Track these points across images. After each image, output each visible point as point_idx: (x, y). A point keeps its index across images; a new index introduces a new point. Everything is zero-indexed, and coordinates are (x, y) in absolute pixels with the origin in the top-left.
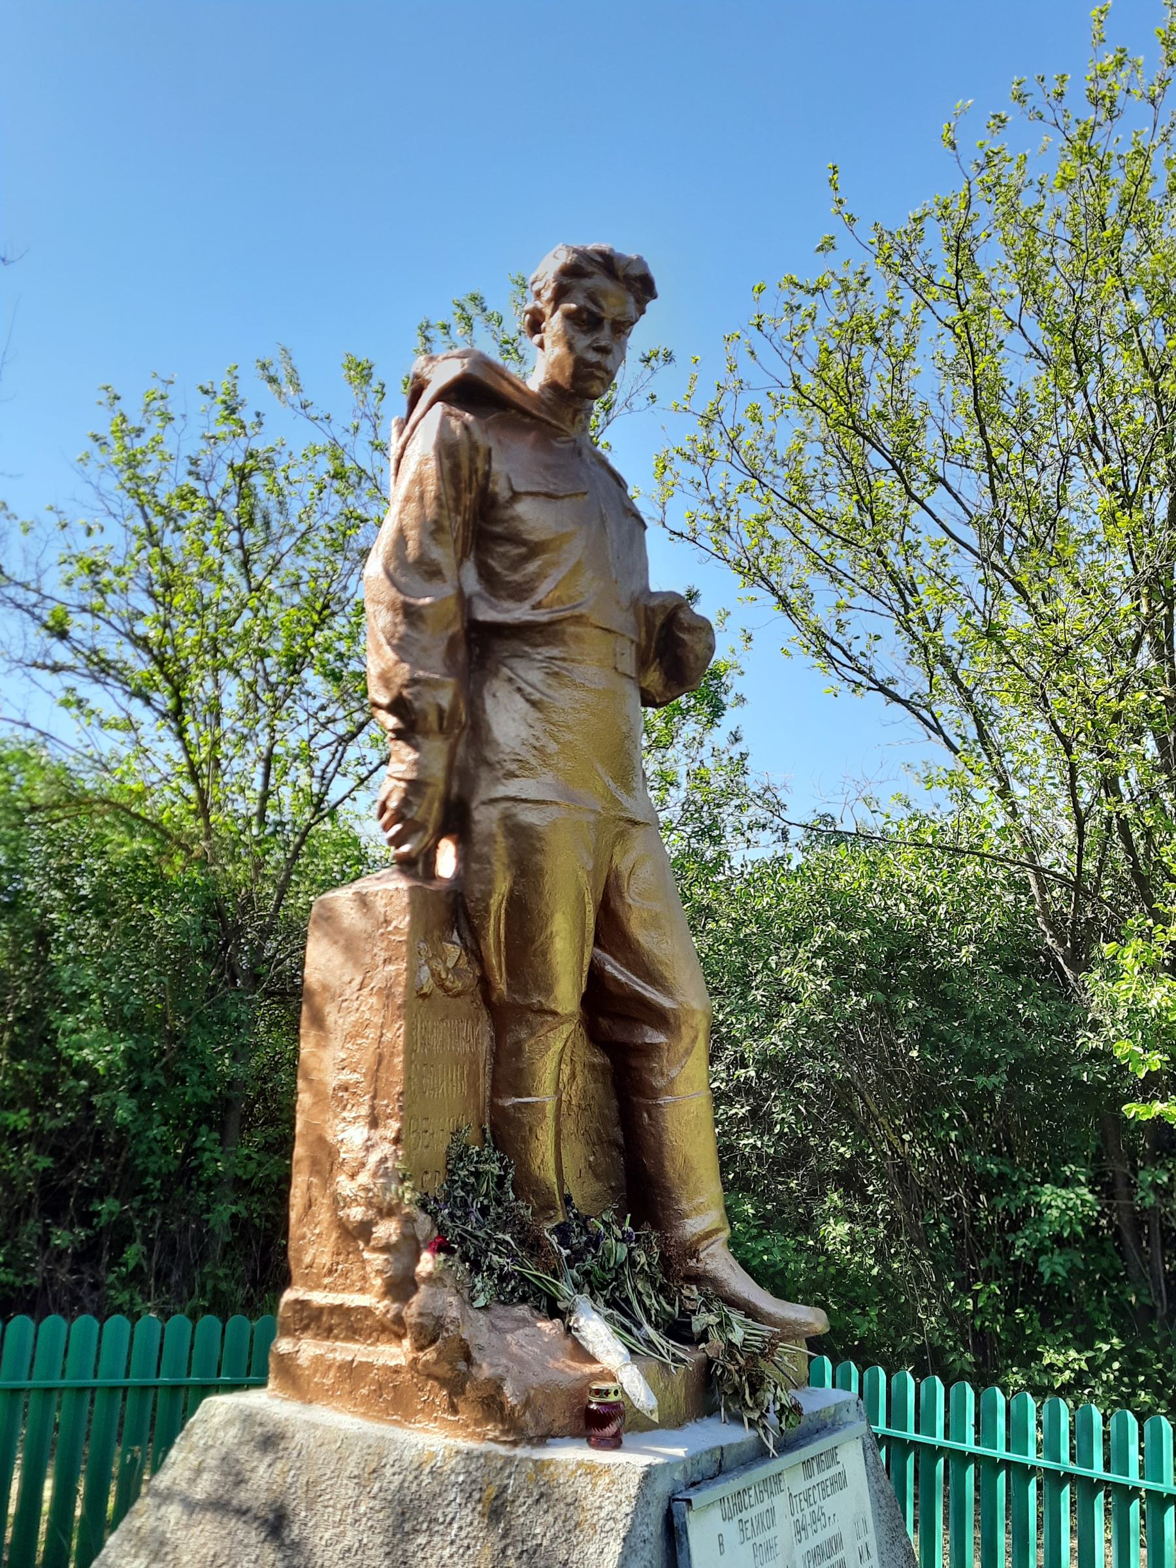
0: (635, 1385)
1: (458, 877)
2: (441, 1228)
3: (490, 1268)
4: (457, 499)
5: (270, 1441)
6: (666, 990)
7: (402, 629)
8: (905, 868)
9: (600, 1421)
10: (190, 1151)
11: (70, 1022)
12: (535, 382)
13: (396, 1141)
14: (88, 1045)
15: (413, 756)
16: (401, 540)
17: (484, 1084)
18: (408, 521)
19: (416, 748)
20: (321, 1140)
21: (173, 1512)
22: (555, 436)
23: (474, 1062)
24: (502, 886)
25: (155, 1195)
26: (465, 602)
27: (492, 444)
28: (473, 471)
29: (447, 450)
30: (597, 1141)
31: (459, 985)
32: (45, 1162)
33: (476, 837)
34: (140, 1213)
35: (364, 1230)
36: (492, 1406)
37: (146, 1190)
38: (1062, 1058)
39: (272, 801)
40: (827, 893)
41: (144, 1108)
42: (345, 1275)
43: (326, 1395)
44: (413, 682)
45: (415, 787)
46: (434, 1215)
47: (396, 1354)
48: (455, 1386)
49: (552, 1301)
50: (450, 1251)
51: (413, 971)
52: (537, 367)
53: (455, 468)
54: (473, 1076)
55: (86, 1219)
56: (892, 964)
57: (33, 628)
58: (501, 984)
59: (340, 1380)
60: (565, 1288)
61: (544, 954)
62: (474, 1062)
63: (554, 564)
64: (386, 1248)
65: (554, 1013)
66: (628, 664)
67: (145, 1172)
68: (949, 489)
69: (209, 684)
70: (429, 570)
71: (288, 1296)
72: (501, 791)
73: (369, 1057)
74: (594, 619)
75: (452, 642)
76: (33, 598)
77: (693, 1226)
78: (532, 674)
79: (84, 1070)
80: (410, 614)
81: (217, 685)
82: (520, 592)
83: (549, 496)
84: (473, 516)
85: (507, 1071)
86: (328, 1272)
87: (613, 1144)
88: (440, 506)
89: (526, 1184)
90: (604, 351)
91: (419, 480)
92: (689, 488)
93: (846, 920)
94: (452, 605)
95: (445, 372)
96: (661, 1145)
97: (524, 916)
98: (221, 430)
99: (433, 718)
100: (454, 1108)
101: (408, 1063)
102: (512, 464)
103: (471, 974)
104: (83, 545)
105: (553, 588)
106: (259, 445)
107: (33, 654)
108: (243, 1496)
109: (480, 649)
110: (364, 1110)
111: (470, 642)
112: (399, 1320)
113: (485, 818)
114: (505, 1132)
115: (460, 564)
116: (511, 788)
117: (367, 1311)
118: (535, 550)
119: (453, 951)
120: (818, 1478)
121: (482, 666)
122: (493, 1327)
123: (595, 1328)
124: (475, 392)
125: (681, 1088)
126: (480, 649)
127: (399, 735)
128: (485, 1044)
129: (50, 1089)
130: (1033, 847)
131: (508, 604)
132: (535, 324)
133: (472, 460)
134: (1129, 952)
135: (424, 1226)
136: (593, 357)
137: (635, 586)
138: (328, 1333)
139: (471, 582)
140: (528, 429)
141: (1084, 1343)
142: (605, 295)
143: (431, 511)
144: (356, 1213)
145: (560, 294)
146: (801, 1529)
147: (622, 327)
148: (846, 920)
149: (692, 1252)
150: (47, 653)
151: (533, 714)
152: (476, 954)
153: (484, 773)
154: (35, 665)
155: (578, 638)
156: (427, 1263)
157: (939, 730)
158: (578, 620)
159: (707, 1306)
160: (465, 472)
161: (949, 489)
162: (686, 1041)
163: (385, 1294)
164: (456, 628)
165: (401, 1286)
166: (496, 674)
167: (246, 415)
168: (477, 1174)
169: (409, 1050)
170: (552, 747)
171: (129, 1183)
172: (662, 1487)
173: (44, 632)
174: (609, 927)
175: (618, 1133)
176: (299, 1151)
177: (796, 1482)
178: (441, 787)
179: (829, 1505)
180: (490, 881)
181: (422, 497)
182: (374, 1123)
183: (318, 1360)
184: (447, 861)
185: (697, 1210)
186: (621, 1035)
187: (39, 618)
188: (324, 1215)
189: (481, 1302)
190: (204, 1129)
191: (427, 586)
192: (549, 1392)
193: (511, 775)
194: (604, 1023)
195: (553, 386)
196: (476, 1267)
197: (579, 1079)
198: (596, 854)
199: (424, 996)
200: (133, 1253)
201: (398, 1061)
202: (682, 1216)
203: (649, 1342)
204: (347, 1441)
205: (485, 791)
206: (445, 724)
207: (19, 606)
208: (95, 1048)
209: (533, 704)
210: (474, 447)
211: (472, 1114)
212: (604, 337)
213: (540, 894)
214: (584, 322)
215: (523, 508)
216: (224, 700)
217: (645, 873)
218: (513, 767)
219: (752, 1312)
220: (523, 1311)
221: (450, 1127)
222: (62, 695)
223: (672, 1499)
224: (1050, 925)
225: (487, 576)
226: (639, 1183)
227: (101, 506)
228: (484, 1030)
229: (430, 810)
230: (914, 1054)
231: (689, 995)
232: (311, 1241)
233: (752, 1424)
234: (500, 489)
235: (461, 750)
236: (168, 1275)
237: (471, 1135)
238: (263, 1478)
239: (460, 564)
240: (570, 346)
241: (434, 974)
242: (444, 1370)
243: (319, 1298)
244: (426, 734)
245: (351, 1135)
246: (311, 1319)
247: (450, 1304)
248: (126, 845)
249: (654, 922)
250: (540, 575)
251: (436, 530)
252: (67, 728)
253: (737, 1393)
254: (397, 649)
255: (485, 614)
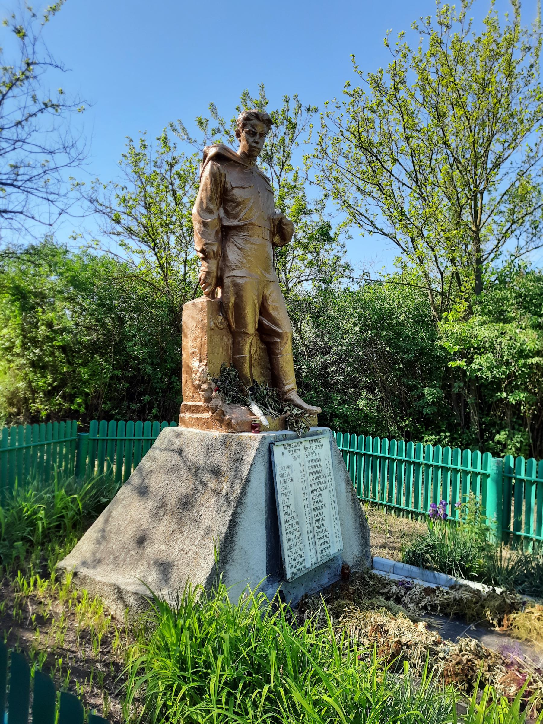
0: (264, 420)
1: (222, 298)
2: (218, 386)
3: (230, 395)
4: (217, 190)
5: (179, 435)
6: (279, 327)
7: (202, 228)
8: (385, 290)
9: (255, 427)
10: (170, 383)
11: (130, 344)
12: (239, 152)
13: (206, 365)
14: (136, 351)
15: (207, 265)
16: (201, 202)
17: (230, 352)
18: (203, 196)
19: (208, 262)
20: (188, 366)
21: (157, 452)
22: (244, 169)
23: (227, 346)
24: (232, 301)
25: (160, 394)
26: (220, 219)
27: (226, 173)
28: (221, 181)
29: (213, 175)
30: (263, 367)
31: (222, 326)
32: (127, 385)
33: (225, 287)
34: (156, 399)
35: (199, 387)
36: (229, 425)
37: (157, 393)
38: (433, 348)
39: (187, 275)
40: (360, 300)
41: (155, 369)
42: (196, 398)
43: (192, 425)
44: (206, 244)
45: (208, 273)
46: (216, 383)
47: (208, 415)
48: (221, 421)
49: (246, 402)
50: (219, 391)
51: (209, 322)
52: (238, 148)
53: (216, 180)
54: (227, 350)
55: (140, 401)
56: (380, 321)
57: (109, 220)
58: (234, 326)
59: (195, 422)
60: (249, 400)
61: (244, 318)
62: (227, 345)
63: (245, 208)
64: (204, 391)
65: (248, 334)
66: (267, 235)
67: (157, 388)
68: (400, 164)
69: (165, 238)
70: (209, 211)
71: (183, 403)
72: (231, 274)
73: (199, 344)
74: (256, 223)
75: (217, 232)
76: (108, 210)
77: (287, 387)
78: (239, 240)
79: (136, 358)
80: (205, 224)
81: (168, 237)
82: (235, 217)
83: (242, 188)
84: (222, 195)
85: (237, 349)
86: (191, 396)
87: (268, 368)
88: (212, 192)
89: (242, 376)
90: (257, 143)
91: (206, 184)
92: (316, 167)
93: (365, 308)
94: (216, 221)
95: (212, 151)
96: (279, 367)
97: (239, 308)
98: (163, 150)
99: (212, 254)
100: (221, 357)
101: (208, 346)
102: (232, 178)
103: (225, 324)
104: (122, 194)
105: (245, 214)
106: (175, 155)
107: (109, 230)
108: (173, 447)
109: (225, 233)
110: (198, 358)
111: (222, 231)
112: (208, 407)
113: (227, 281)
114: (236, 364)
115: (218, 209)
116: (234, 273)
117: (201, 406)
118: (238, 204)
119: (220, 318)
120: (313, 444)
121: (226, 238)
122: (230, 408)
123: (255, 408)
124: (221, 157)
125: (284, 353)
126: (225, 233)
127: (203, 259)
128: (231, 342)
129: (127, 363)
130: (430, 283)
131: (232, 220)
132: (238, 135)
133: (220, 178)
134: (450, 315)
135: (213, 385)
136: (254, 145)
137: (270, 212)
138: (192, 412)
139: (222, 214)
140: (237, 167)
141: (438, 434)
142: (256, 126)
143: (209, 194)
144: (197, 383)
145: (244, 126)
146: (307, 455)
147: (262, 135)
148: (365, 308)
149: (286, 393)
150: (114, 229)
151: (239, 252)
152: (226, 318)
153: (227, 269)
154: (110, 233)
155: (252, 229)
156: (214, 394)
157: (399, 245)
158: (252, 224)
159: (289, 406)
160: (218, 182)
161: (400, 164)
162: (285, 340)
163: (204, 402)
164: (218, 227)
165: (208, 400)
166: (229, 241)
167: (171, 144)
168: (229, 374)
169: (209, 343)
170: (245, 261)
171: (152, 391)
172: (268, 441)
173: (113, 222)
174: (263, 310)
175: (269, 365)
176: (183, 369)
177: (307, 444)
178: (215, 274)
179: (317, 451)
180: (229, 299)
181: (206, 189)
182: (201, 361)
183: (190, 418)
184: (219, 294)
185: (288, 384)
186: (268, 340)
187: (110, 217)
188: (190, 384)
189: (228, 402)
190: (173, 376)
191: (209, 216)
192: (243, 422)
193: (234, 269)
194: (264, 336)
195: (243, 153)
196: (226, 394)
197: (258, 351)
198: (258, 290)
199: (212, 329)
200: (155, 411)
201: (206, 345)
202: (284, 385)
203: (271, 413)
204: (196, 435)
205: (227, 275)
206: (216, 255)
207: (104, 213)
208: (140, 353)
209: (239, 249)
210: (221, 174)
211: (227, 359)
212: (257, 138)
213: (243, 302)
214: (251, 134)
215: (236, 192)
216: (170, 242)
217: (274, 295)
218: (234, 267)
219: (301, 408)
220: (238, 405)
221: (221, 362)
222: (120, 242)
223: (270, 443)
224: (434, 308)
225: (226, 212)
226: (275, 379)
227: (127, 178)
228: (230, 338)
229: (213, 280)
230: (388, 349)
231: (286, 326)
232: (187, 391)
233: (295, 431)
234: (228, 186)
235: (220, 262)
236: (166, 417)
237: (227, 365)
238: (177, 443)
239: (218, 209)
240: (248, 142)
241: (215, 324)
242: (218, 418)
243: (190, 404)
244: (210, 259)
245: (195, 364)
246: (189, 409)
247: (219, 403)
248: (142, 290)
249: (276, 309)
250: (241, 211)
251: (211, 199)
252: (122, 253)
253: (292, 424)
254: (201, 234)
255: (226, 223)
